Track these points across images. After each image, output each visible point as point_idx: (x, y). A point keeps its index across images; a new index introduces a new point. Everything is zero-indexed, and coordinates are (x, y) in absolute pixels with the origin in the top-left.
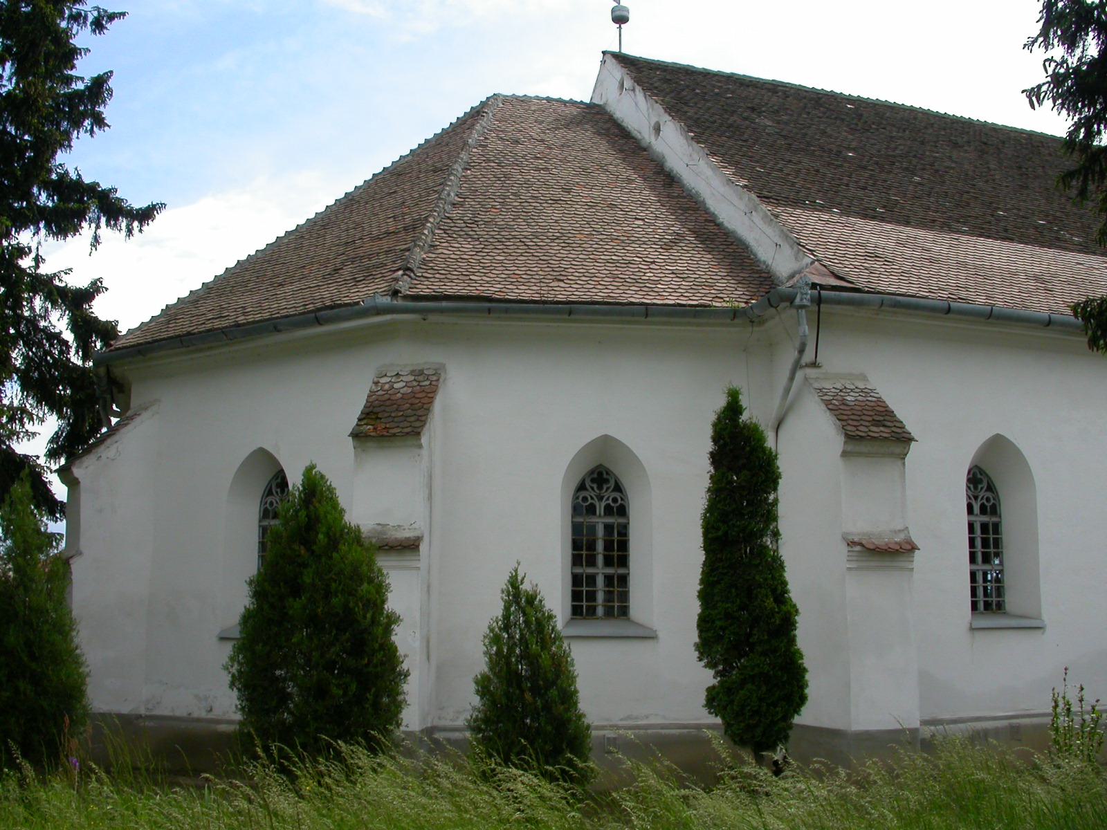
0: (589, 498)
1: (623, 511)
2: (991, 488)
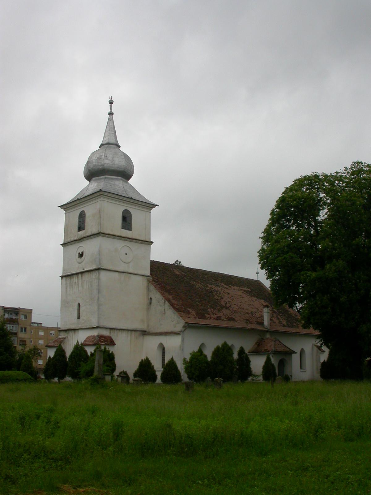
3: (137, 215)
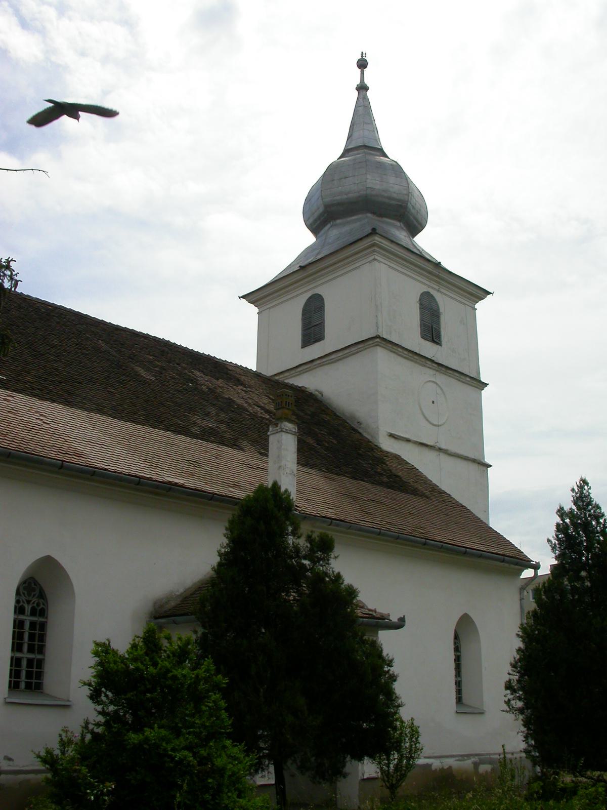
0: (21, 602)
1: (43, 613)
2: (42, 595)
3: (448, 305)
